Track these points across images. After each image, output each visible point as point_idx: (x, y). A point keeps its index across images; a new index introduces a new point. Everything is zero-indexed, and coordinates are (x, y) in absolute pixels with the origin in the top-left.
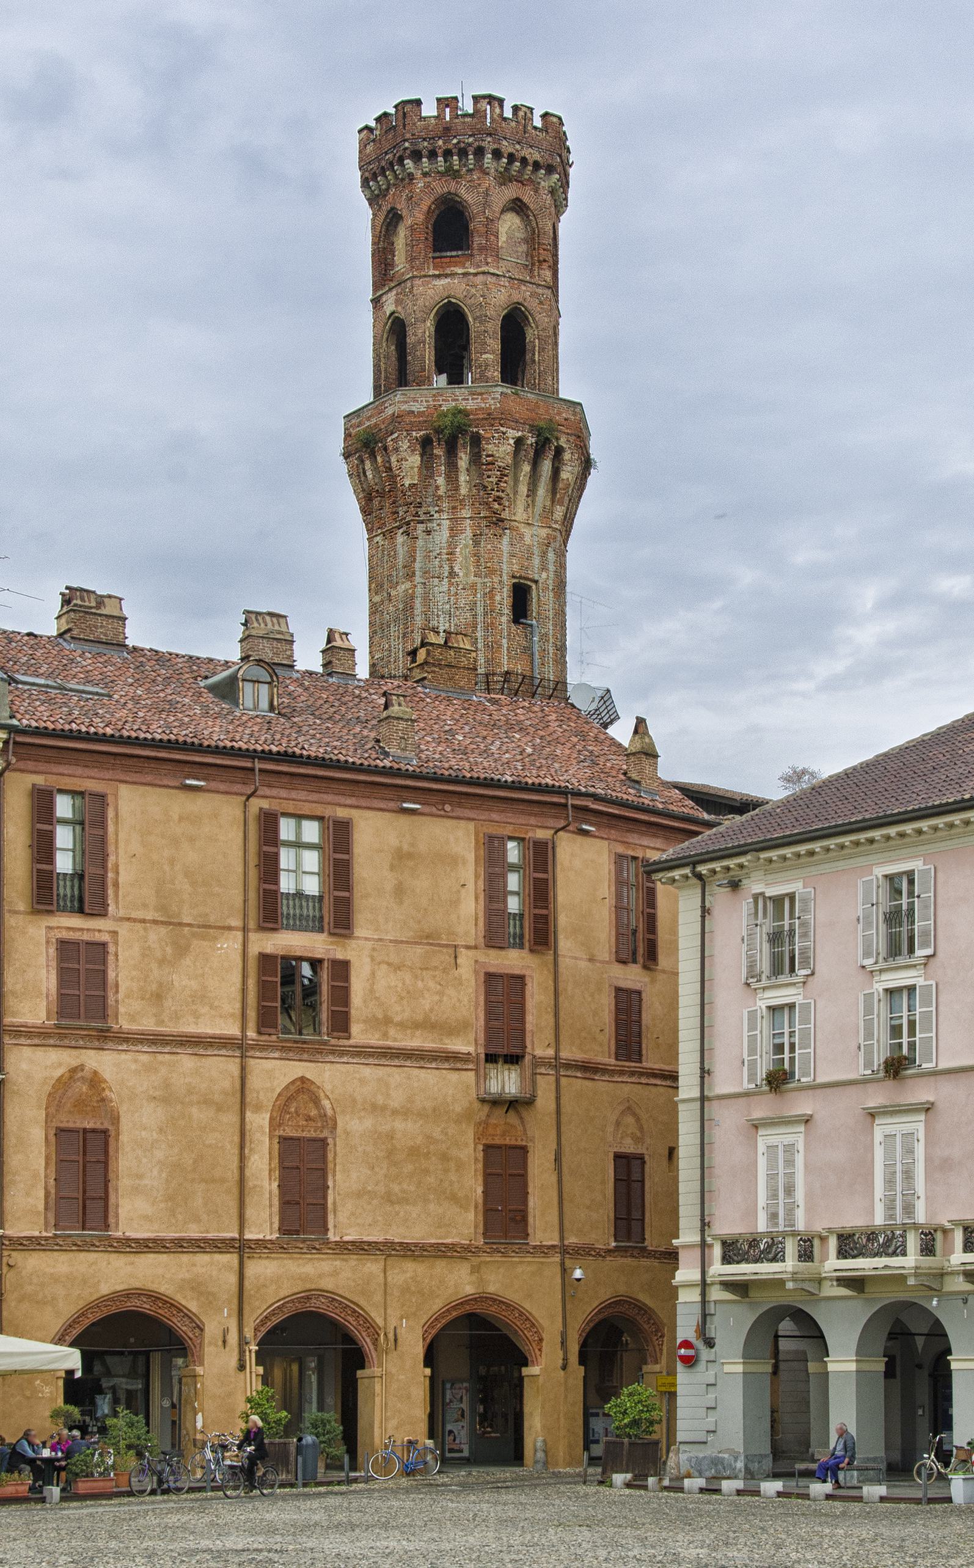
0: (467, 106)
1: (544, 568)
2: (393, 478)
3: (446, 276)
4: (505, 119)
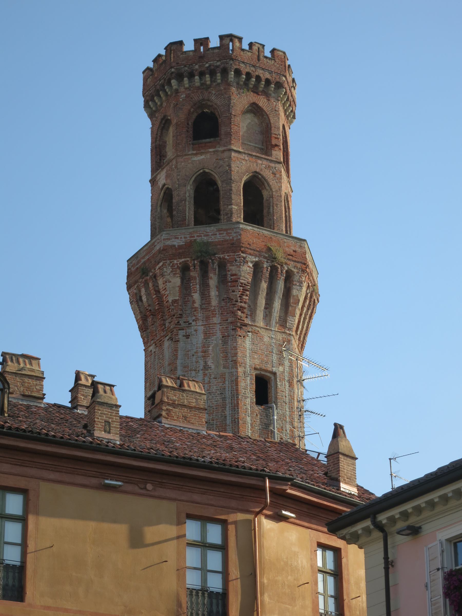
0: (214, 43)
1: (281, 364)
4: (243, 50)
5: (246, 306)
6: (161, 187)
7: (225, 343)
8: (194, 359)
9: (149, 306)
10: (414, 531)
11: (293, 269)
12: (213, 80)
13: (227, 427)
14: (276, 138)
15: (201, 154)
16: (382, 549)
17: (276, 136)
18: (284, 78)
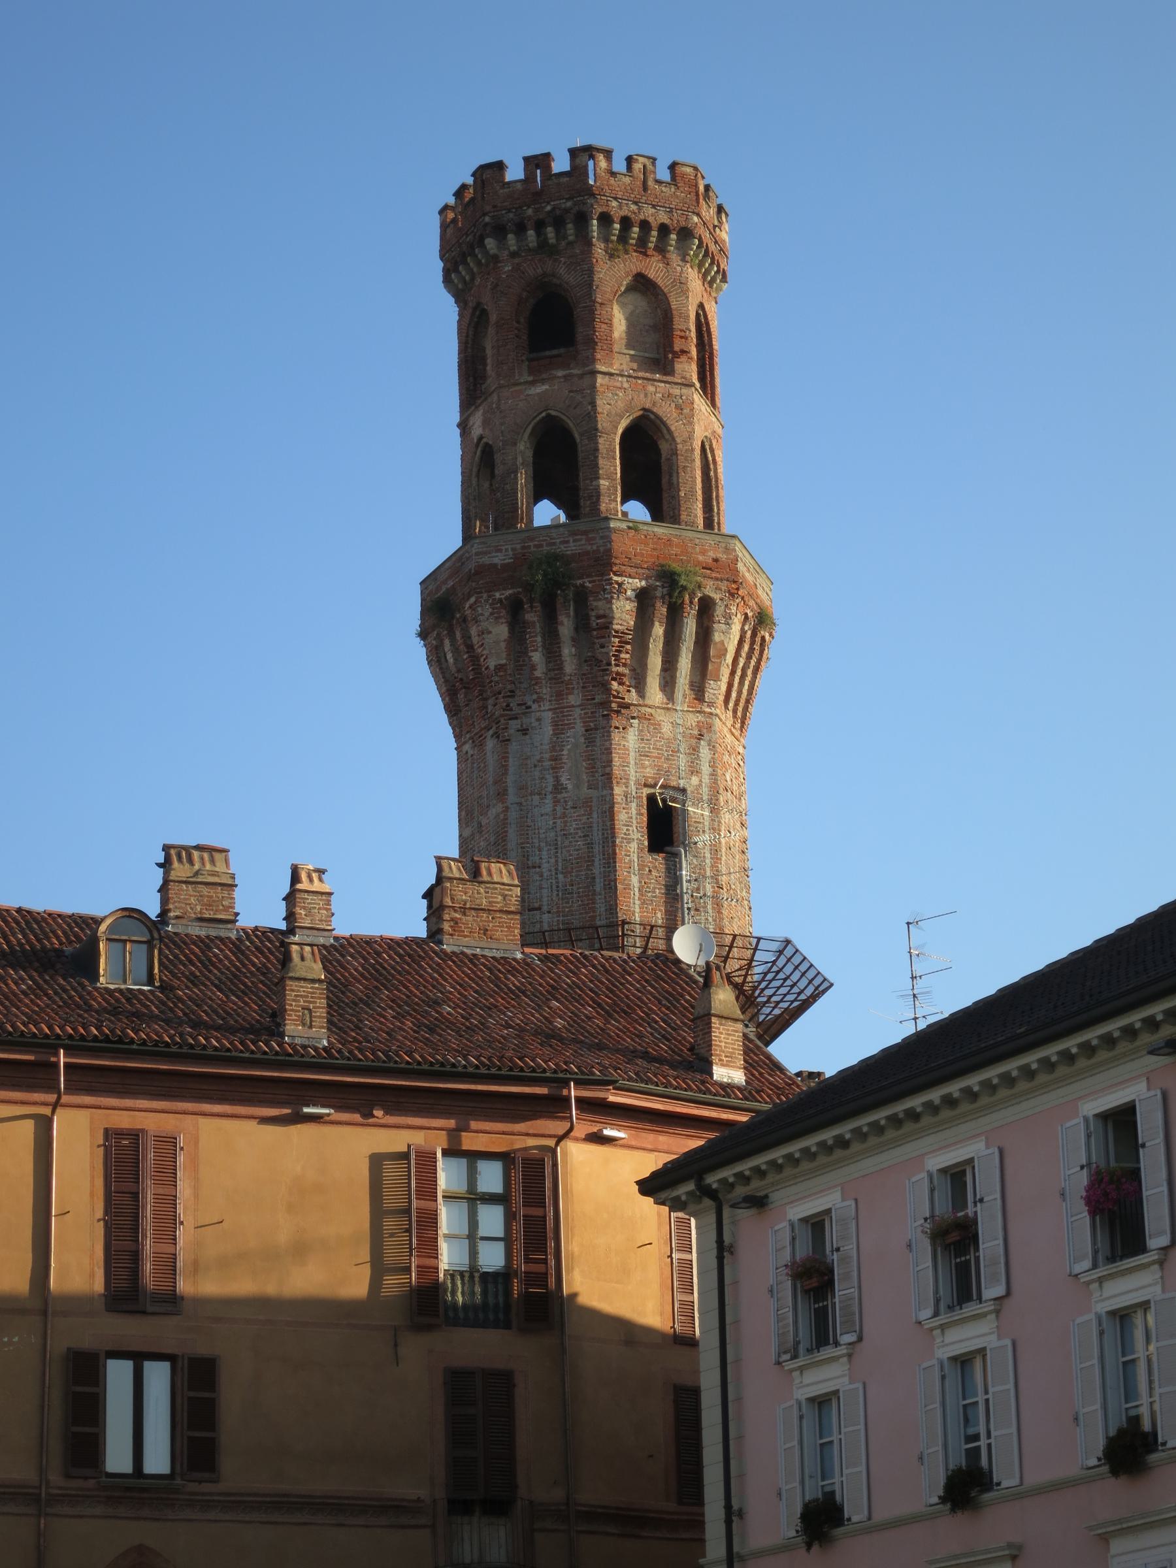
1: (694, 771)
2: (475, 659)
4: (613, 174)
5: (626, 671)
7: (590, 741)
9: (459, 671)
10: (759, 1203)
11: (712, 595)
12: (560, 235)
13: (597, 897)
14: (681, 337)
15: (543, 381)
16: (714, 1226)
17: (682, 334)
18: (696, 219)
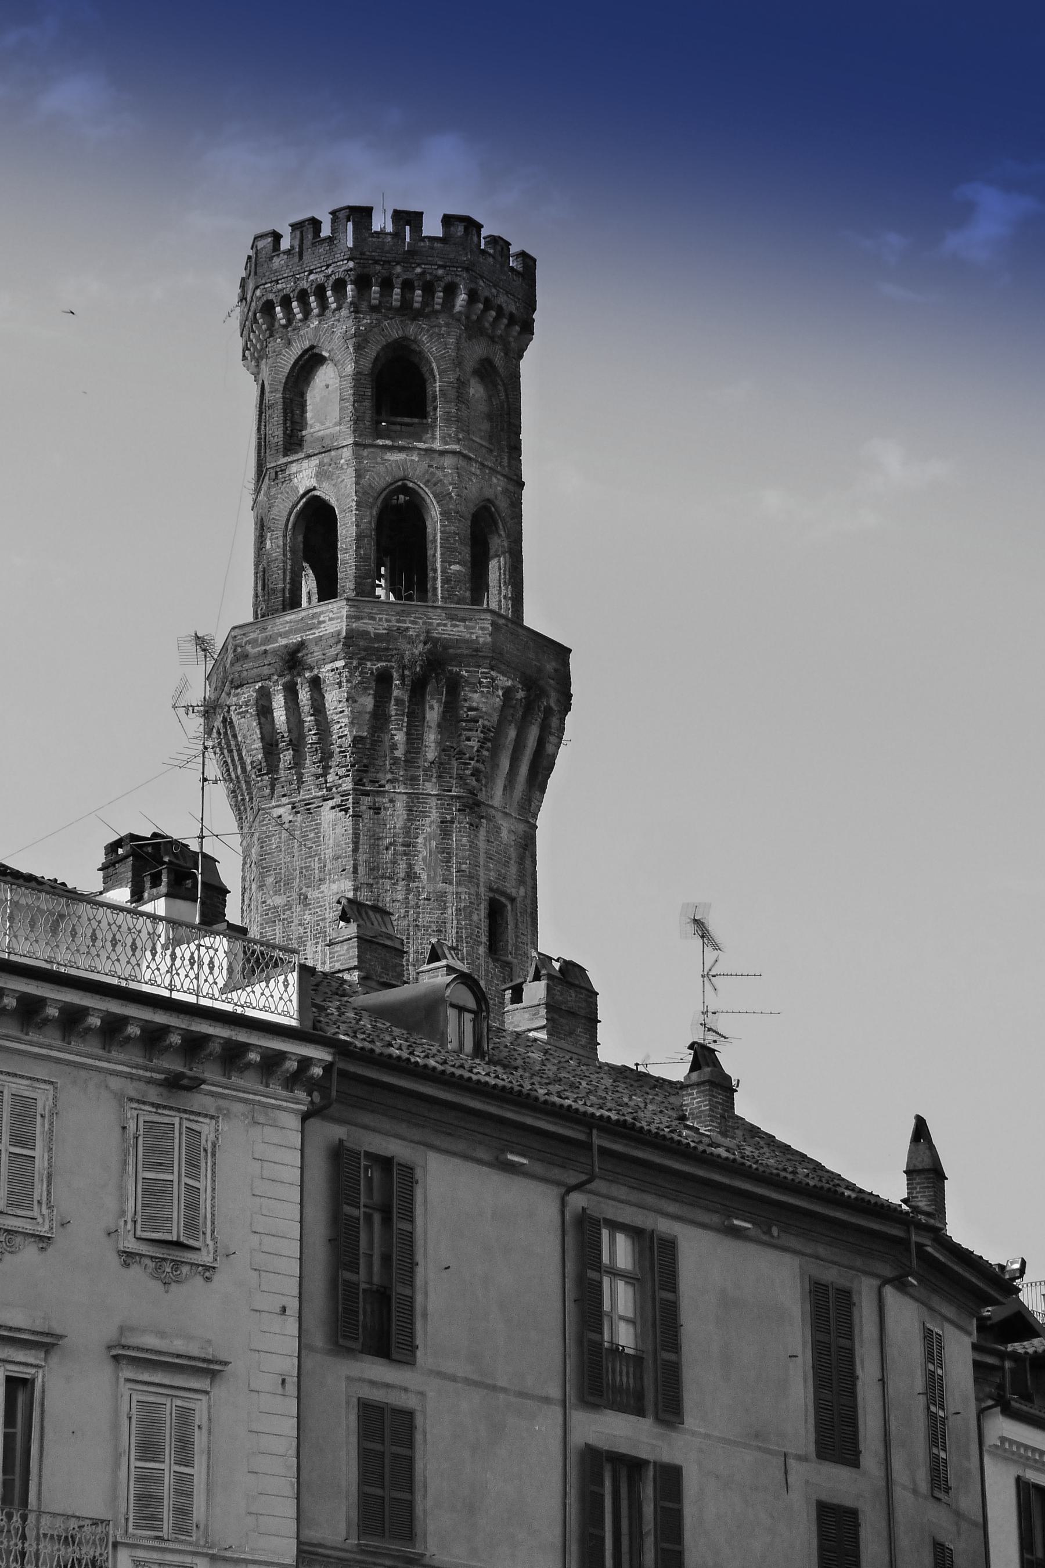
3: (401, 449)
6: (301, 492)
8: (389, 855)
